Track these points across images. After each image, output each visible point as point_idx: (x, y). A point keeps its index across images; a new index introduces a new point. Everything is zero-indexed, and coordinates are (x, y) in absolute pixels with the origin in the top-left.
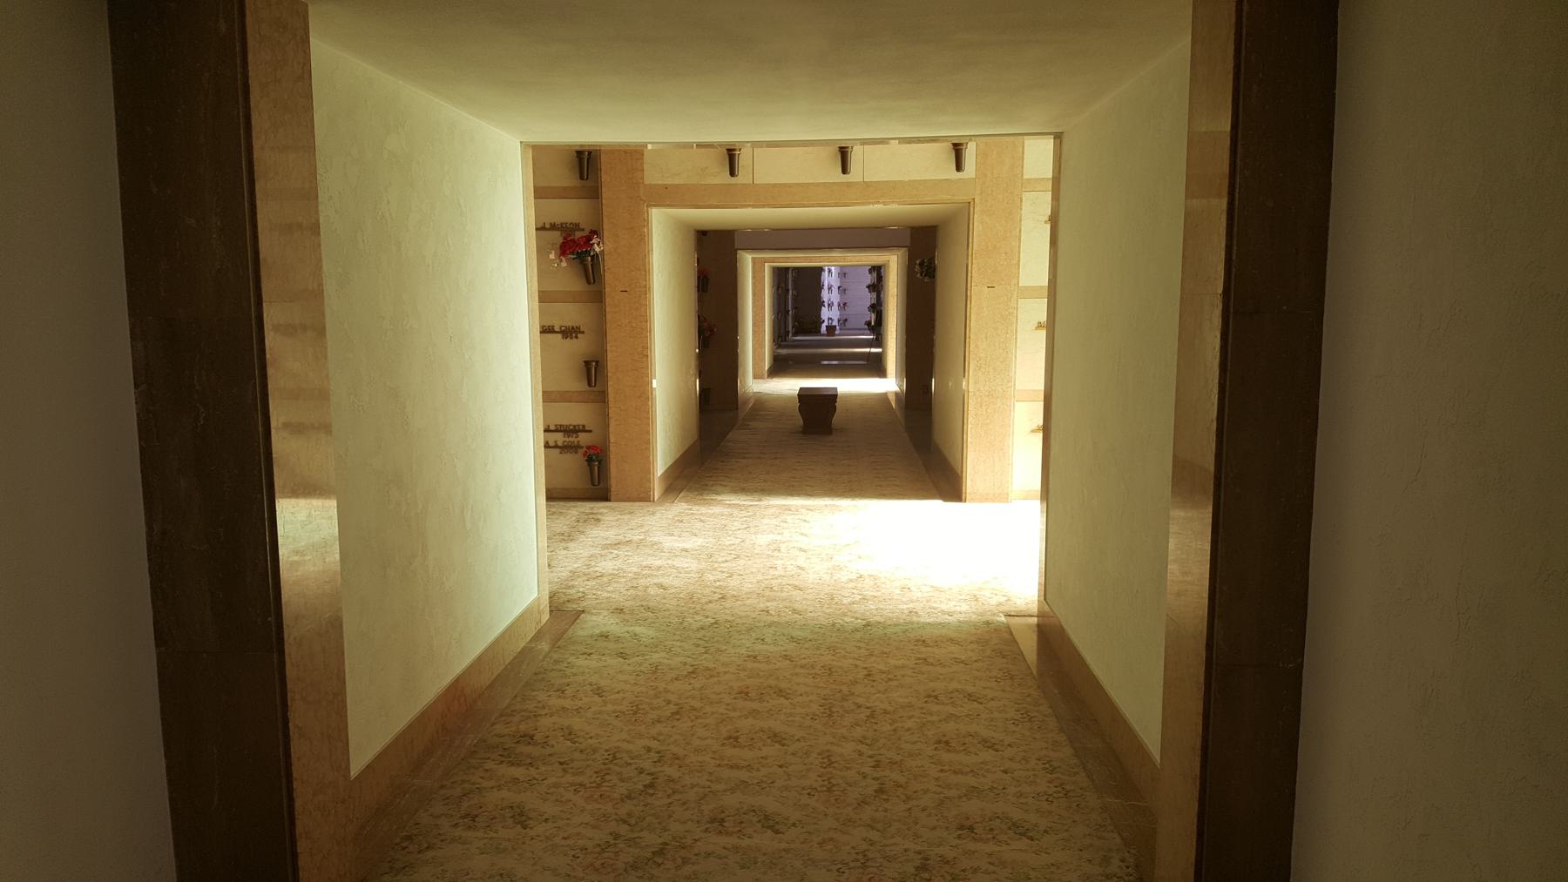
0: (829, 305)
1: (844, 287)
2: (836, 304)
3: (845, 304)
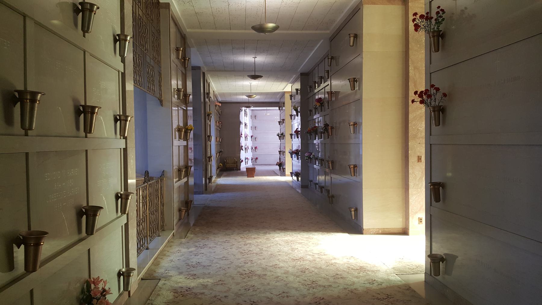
0: (246, 149)
1: (255, 136)
2: (250, 148)
3: (256, 148)
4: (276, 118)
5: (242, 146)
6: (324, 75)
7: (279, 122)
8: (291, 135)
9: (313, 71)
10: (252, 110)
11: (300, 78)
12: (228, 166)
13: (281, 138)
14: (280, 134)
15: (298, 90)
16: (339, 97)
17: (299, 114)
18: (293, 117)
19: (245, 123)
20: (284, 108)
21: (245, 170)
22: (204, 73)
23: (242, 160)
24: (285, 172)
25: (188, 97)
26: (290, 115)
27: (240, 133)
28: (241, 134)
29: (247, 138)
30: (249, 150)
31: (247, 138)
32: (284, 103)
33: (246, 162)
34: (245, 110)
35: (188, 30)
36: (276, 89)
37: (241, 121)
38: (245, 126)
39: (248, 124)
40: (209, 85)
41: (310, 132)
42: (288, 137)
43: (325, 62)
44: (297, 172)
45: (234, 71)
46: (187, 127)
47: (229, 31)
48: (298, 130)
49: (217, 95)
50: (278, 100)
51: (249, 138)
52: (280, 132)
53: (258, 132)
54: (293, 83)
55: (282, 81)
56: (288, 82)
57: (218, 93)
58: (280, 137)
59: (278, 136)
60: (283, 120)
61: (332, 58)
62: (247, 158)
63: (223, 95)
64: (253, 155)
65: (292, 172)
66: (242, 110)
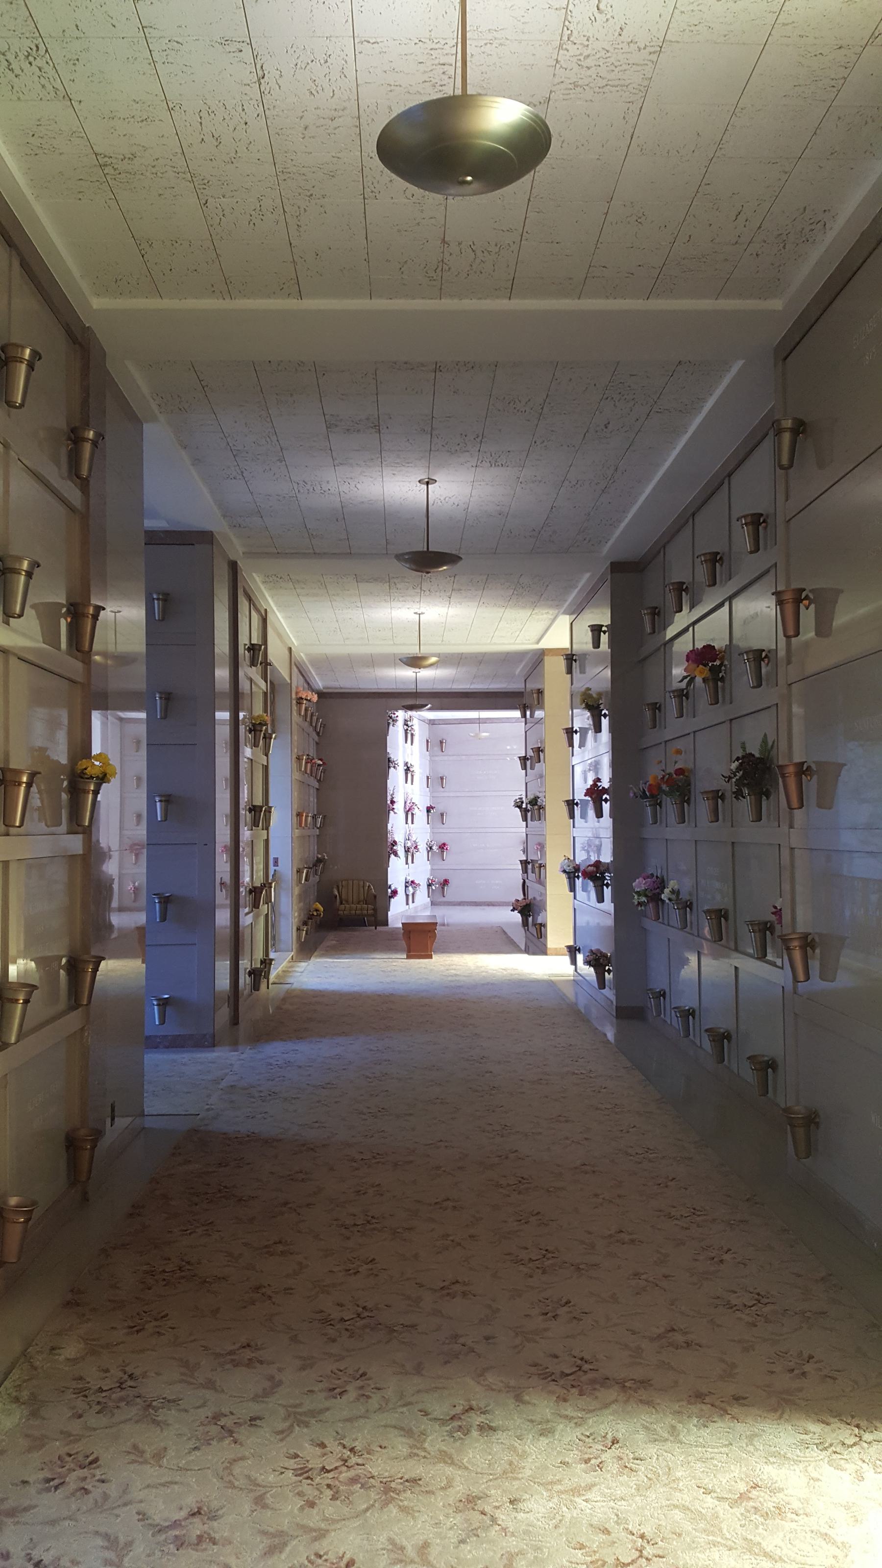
0: (407, 850)
1: (440, 808)
2: (422, 847)
3: (443, 847)
4: (508, 747)
5: (395, 843)
6: (691, 580)
7: (524, 760)
8: (571, 804)
9: (664, 547)
10: (432, 722)
11: (608, 583)
12: (345, 910)
13: (529, 814)
14: (524, 799)
15: (601, 631)
16: (834, 624)
17: (605, 722)
18: (576, 738)
19: (406, 764)
20: (539, 714)
21: (401, 926)
22: (233, 567)
23: (393, 888)
24: (546, 937)
25: (89, 622)
26: (566, 729)
27: (389, 798)
28: (393, 802)
29: (413, 814)
30: (421, 856)
31: (413, 814)
32: (540, 692)
33: (407, 896)
34: (406, 721)
35: (97, 303)
36: (512, 641)
37: (393, 757)
38: (406, 774)
39: (417, 769)
40: (264, 621)
41: (654, 796)
42: (555, 810)
43: (729, 488)
44: (598, 950)
45: (349, 555)
46: (83, 764)
47: (291, 304)
48: (599, 784)
49: (305, 663)
50: (516, 686)
51: (420, 815)
52: (524, 793)
53: (452, 794)
54: (577, 610)
55: (534, 605)
56: (557, 606)
57: (306, 655)
58: (525, 813)
59: (520, 807)
60: (539, 751)
61: (800, 428)
62: (412, 882)
63: (326, 663)
64: (432, 869)
65: (571, 943)
66: (397, 721)
